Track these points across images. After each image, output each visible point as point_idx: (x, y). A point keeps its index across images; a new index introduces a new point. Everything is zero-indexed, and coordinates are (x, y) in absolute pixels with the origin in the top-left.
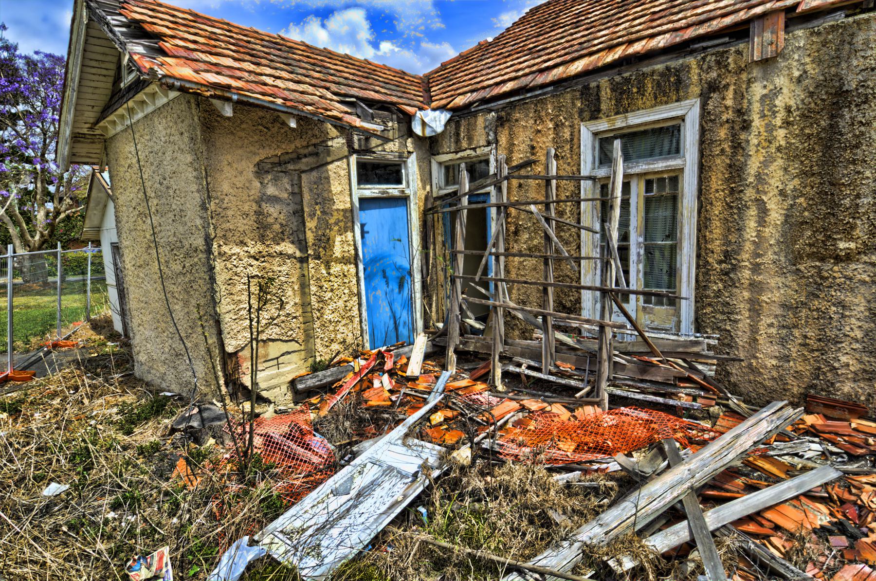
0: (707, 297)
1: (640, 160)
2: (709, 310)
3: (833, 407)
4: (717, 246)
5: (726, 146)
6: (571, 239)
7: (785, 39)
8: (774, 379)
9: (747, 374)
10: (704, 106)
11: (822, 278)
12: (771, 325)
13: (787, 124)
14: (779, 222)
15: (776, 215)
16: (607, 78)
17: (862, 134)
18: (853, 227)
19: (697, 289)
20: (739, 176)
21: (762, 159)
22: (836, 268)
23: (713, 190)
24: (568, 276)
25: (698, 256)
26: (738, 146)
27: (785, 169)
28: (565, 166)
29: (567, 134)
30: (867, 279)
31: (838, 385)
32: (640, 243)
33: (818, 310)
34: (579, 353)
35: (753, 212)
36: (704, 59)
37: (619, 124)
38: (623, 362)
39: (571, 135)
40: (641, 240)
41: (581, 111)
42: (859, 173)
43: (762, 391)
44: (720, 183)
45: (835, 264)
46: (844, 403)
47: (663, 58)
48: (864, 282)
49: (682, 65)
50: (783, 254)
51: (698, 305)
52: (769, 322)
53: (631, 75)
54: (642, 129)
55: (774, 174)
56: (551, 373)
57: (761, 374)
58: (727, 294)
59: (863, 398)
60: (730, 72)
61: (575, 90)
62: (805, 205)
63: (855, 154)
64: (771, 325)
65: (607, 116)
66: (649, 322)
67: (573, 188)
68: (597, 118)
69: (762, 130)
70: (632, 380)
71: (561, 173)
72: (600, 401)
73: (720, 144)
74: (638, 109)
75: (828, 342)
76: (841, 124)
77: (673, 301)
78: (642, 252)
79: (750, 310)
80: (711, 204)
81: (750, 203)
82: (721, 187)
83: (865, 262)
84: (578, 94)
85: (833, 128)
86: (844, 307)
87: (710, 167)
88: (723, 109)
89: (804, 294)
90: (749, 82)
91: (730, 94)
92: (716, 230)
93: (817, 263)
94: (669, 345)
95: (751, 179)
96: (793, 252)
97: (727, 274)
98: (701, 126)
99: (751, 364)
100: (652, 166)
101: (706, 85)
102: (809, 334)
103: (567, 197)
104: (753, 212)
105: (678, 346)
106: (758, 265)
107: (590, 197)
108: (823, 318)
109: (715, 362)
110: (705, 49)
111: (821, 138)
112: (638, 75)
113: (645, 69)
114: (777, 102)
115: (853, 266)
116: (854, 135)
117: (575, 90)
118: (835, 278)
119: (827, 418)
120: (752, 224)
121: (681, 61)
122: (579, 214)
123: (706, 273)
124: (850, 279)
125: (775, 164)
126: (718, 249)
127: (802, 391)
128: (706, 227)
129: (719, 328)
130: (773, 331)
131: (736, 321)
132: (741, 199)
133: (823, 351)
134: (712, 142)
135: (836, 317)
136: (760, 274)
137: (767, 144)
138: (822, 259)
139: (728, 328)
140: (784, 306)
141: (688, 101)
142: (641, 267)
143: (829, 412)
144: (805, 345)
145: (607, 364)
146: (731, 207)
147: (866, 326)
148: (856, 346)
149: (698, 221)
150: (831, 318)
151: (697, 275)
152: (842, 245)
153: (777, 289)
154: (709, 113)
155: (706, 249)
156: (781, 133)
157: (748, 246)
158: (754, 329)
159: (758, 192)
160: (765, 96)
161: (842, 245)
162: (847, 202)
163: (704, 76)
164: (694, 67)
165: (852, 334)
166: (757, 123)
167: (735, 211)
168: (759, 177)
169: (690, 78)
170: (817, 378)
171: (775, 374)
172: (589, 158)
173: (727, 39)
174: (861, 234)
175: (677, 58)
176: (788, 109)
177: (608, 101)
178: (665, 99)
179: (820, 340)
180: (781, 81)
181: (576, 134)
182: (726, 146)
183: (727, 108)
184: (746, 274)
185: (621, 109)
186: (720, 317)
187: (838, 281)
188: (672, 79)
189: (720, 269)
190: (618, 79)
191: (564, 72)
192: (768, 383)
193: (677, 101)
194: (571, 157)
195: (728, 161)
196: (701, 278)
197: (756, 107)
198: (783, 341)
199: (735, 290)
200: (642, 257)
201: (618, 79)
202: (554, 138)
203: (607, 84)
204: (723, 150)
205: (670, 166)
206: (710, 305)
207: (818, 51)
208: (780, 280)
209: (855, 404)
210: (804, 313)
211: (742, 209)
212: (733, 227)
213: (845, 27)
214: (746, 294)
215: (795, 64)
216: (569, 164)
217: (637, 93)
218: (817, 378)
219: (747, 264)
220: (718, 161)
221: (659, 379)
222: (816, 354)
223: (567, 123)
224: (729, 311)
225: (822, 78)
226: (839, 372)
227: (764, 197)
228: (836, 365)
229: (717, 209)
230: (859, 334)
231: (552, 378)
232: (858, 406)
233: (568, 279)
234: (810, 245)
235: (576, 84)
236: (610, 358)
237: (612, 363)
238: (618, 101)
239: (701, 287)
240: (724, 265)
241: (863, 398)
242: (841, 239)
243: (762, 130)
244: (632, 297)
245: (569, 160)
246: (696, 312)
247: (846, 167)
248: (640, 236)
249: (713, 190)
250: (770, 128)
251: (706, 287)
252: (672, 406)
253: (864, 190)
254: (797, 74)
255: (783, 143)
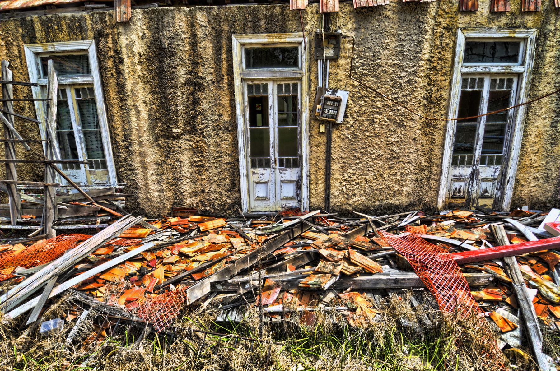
0: (120, 161)
1: (69, 75)
2: (123, 169)
3: (184, 212)
4: (119, 131)
5: (113, 71)
6: (33, 128)
7: (132, 12)
8: (159, 203)
9: (147, 202)
10: (97, 45)
11: (169, 148)
12: (152, 175)
13: (141, 63)
14: (146, 118)
15: (144, 115)
16: (37, 16)
17: (174, 73)
18: (177, 121)
19: (114, 157)
20: (123, 91)
21: (132, 82)
22: (174, 143)
23: (111, 98)
24: (36, 154)
25: (111, 138)
26: (119, 73)
27: (144, 89)
28: (19, 74)
29: (16, 52)
30: (187, 147)
31: (184, 201)
32: (79, 130)
33: (170, 164)
34: (39, 206)
35: (133, 112)
36: (93, 15)
37: (50, 49)
38: (65, 207)
39: (19, 52)
40: (80, 128)
41: (23, 36)
42: (175, 93)
43: (155, 210)
44: (114, 94)
45: (173, 140)
46: (188, 209)
47: (70, 9)
48: (186, 149)
49: (81, 16)
50: (151, 136)
51: (117, 167)
52: (151, 173)
53: (52, 17)
54: (66, 54)
55: (139, 91)
56: (18, 224)
57: (153, 201)
58: (130, 159)
59: (195, 205)
60: (108, 26)
61: (16, 20)
62: (156, 109)
63: (172, 83)
64: (152, 175)
65: (42, 42)
66: (94, 180)
67: (27, 91)
68: (35, 43)
69: (129, 65)
70: (71, 217)
71: (17, 80)
72: (47, 236)
73: (110, 70)
74: (60, 41)
75: (177, 180)
76: (164, 66)
77: (104, 166)
78: (82, 136)
79: (142, 167)
80: (112, 106)
81: (131, 107)
82: (115, 97)
83: (185, 139)
84: (19, 23)
85: (161, 67)
86: (180, 162)
87: (107, 84)
88: (108, 49)
89: (164, 156)
90: (119, 34)
91: (110, 40)
92: (118, 123)
93: (166, 140)
94: (96, 192)
95: (129, 93)
96: (155, 134)
97: (127, 148)
98: (98, 57)
99: (147, 197)
100: (75, 80)
101: (96, 32)
102: (169, 177)
103: (24, 97)
104: (133, 112)
105: (101, 192)
106: (141, 142)
107: (40, 98)
108: (173, 168)
109: (124, 198)
110: (93, 8)
111: (157, 73)
112: (56, 18)
113: (60, 15)
114: (134, 49)
115: (181, 141)
116: (171, 73)
117: (16, 20)
118: (174, 148)
119: (181, 217)
120: (134, 119)
121: (80, 14)
122: (35, 110)
123: (117, 148)
124: (181, 148)
125: (139, 85)
126: (120, 134)
127: (171, 206)
128: (112, 120)
129: (129, 179)
130: (154, 177)
131: (136, 174)
132: (126, 104)
133: (175, 185)
134: (106, 69)
135: (178, 167)
136: (143, 147)
137: (133, 73)
138: (168, 138)
139: (134, 178)
140: (156, 164)
141: (87, 41)
142: (83, 145)
143: (182, 215)
144: (168, 183)
145: (52, 210)
146: (122, 109)
147: (190, 170)
148: (188, 180)
149: (108, 117)
150: (176, 168)
151: (113, 149)
152: (174, 130)
153: (152, 155)
154: (101, 50)
155: (115, 133)
156: (139, 67)
157: (135, 132)
158: (146, 178)
159: (134, 101)
160: (127, 44)
161: (174, 130)
162: (172, 108)
163: (94, 26)
164: (88, 19)
165: (185, 175)
166: (126, 60)
167: (125, 111)
168: (132, 91)
169: (87, 26)
170: (176, 199)
171: (159, 200)
172: (35, 71)
173: (104, 5)
174: (181, 125)
175: (79, 11)
176: (140, 54)
177: (40, 32)
178: (75, 37)
179: (174, 180)
180: (134, 37)
181: (22, 52)
182: (113, 72)
183: (110, 48)
184: (136, 148)
185: (50, 39)
186: (129, 173)
187: (176, 149)
188: (77, 25)
189: (123, 146)
190: (44, 17)
191: (8, 5)
192: (157, 205)
193: (82, 39)
194: (22, 69)
195: (116, 81)
196: (115, 151)
197: (124, 50)
198: (159, 182)
199: (133, 157)
200: (82, 139)
201: (44, 17)
202: (7, 53)
203: (37, 20)
204: (112, 74)
205: (85, 81)
206: (123, 166)
207: (148, 23)
208: (152, 150)
209: (192, 209)
210: (165, 166)
211: (128, 110)
212: (126, 121)
213: (158, 11)
214: (139, 159)
215: (139, 28)
216: (21, 73)
217: (58, 29)
218: (176, 199)
219: (136, 141)
220: (111, 81)
221: (85, 214)
222: (174, 187)
223: (14, 43)
224: (133, 169)
225: (152, 39)
226: (184, 194)
227: (137, 104)
228: (182, 191)
229: (116, 110)
230: (188, 175)
231: (19, 227)
232: (193, 209)
233: (36, 156)
234: (162, 131)
235: (17, 16)
236: (54, 207)
237: (56, 210)
238: (47, 33)
239: (116, 156)
240: (125, 143)
241: (195, 205)
242: (173, 128)
243: (129, 65)
244: (82, 166)
245: (21, 71)
246: (117, 171)
247: (170, 90)
248: (79, 125)
249: (111, 98)
250: (133, 65)
251: (119, 156)
252: (93, 228)
253: (179, 102)
254: (141, 34)
255: (140, 73)
